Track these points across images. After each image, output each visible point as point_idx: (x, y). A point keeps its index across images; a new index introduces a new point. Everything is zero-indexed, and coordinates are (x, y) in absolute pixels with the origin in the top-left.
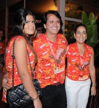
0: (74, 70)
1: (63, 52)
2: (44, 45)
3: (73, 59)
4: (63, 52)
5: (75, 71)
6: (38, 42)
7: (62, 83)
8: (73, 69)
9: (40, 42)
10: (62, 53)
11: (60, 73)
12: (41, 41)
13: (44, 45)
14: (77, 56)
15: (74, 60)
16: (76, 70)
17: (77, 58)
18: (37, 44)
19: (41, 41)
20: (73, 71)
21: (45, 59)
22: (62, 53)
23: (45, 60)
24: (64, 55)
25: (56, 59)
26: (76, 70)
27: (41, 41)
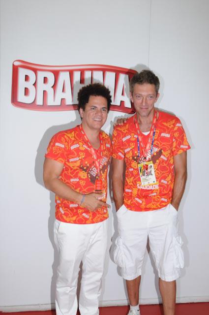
0: (76, 177)
1: (155, 154)
2: (128, 137)
3: (126, 148)
4: (155, 154)
5: (77, 180)
6: (123, 131)
7: (49, 308)
8: (72, 176)
9: (126, 131)
10: (154, 155)
11: (154, 190)
12: (128, 130)
13: (128, 137)
14: (133, 142)
15: (128, 149)
16: (80, 179)
17: (133, 146)
18: (121, 133)
19: (127, 129)
20: (72, 180)
21: (70, 168)
22: (154, 155)
23: (71, 169)
24: (157, 161)
25: (91, 175)
26: (80, 179)
27: (128, 130)
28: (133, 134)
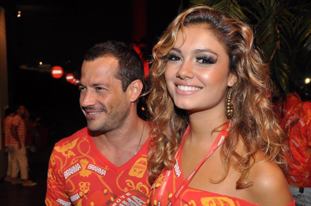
28: (85, 162)
